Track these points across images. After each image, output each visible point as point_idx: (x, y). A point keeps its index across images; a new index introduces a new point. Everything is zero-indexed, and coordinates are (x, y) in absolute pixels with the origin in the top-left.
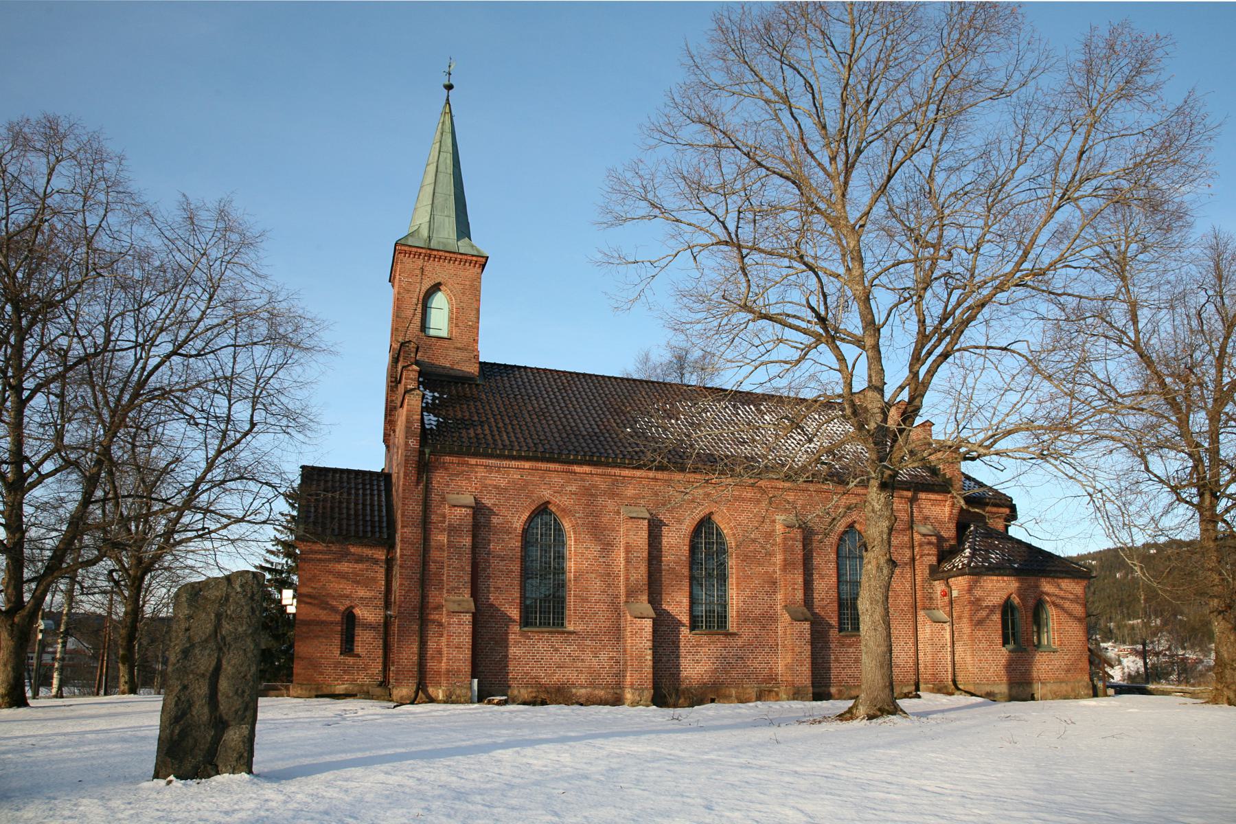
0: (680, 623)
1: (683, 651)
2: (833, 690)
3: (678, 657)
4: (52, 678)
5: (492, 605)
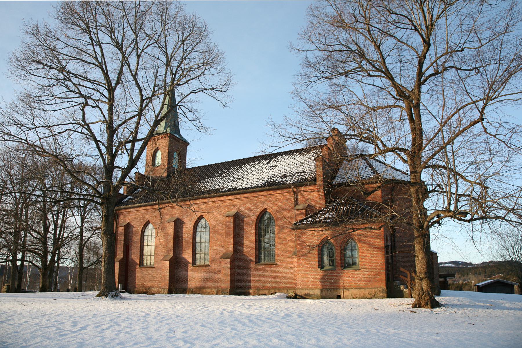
0: (188, 262)
1: (189, 274)
2: (251, 291)
3: (187, 276)
4: (413, 257)
5: (132, 259)
